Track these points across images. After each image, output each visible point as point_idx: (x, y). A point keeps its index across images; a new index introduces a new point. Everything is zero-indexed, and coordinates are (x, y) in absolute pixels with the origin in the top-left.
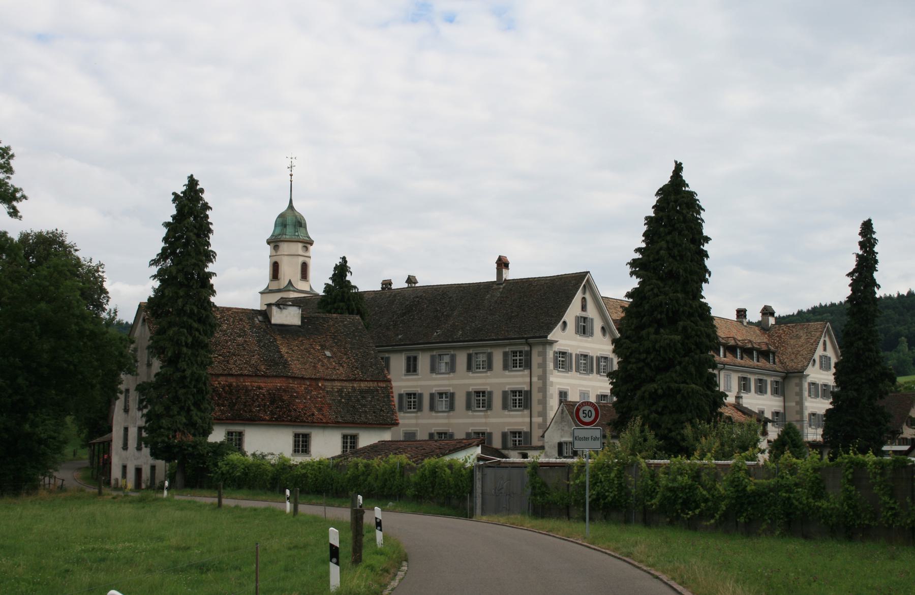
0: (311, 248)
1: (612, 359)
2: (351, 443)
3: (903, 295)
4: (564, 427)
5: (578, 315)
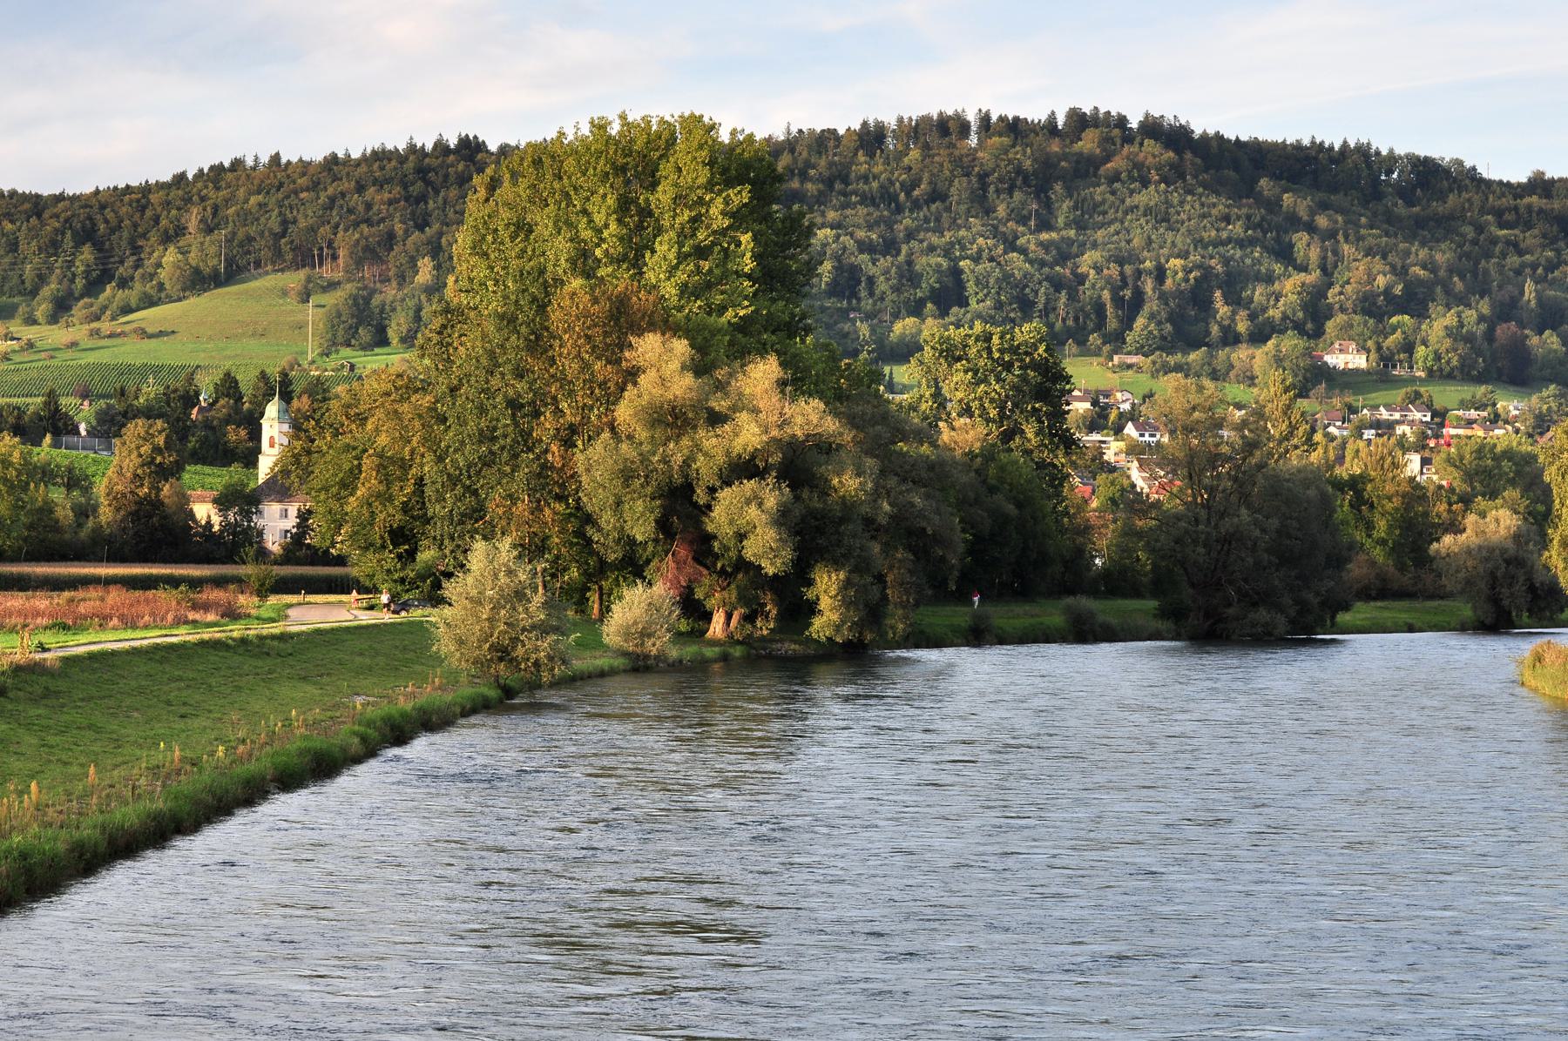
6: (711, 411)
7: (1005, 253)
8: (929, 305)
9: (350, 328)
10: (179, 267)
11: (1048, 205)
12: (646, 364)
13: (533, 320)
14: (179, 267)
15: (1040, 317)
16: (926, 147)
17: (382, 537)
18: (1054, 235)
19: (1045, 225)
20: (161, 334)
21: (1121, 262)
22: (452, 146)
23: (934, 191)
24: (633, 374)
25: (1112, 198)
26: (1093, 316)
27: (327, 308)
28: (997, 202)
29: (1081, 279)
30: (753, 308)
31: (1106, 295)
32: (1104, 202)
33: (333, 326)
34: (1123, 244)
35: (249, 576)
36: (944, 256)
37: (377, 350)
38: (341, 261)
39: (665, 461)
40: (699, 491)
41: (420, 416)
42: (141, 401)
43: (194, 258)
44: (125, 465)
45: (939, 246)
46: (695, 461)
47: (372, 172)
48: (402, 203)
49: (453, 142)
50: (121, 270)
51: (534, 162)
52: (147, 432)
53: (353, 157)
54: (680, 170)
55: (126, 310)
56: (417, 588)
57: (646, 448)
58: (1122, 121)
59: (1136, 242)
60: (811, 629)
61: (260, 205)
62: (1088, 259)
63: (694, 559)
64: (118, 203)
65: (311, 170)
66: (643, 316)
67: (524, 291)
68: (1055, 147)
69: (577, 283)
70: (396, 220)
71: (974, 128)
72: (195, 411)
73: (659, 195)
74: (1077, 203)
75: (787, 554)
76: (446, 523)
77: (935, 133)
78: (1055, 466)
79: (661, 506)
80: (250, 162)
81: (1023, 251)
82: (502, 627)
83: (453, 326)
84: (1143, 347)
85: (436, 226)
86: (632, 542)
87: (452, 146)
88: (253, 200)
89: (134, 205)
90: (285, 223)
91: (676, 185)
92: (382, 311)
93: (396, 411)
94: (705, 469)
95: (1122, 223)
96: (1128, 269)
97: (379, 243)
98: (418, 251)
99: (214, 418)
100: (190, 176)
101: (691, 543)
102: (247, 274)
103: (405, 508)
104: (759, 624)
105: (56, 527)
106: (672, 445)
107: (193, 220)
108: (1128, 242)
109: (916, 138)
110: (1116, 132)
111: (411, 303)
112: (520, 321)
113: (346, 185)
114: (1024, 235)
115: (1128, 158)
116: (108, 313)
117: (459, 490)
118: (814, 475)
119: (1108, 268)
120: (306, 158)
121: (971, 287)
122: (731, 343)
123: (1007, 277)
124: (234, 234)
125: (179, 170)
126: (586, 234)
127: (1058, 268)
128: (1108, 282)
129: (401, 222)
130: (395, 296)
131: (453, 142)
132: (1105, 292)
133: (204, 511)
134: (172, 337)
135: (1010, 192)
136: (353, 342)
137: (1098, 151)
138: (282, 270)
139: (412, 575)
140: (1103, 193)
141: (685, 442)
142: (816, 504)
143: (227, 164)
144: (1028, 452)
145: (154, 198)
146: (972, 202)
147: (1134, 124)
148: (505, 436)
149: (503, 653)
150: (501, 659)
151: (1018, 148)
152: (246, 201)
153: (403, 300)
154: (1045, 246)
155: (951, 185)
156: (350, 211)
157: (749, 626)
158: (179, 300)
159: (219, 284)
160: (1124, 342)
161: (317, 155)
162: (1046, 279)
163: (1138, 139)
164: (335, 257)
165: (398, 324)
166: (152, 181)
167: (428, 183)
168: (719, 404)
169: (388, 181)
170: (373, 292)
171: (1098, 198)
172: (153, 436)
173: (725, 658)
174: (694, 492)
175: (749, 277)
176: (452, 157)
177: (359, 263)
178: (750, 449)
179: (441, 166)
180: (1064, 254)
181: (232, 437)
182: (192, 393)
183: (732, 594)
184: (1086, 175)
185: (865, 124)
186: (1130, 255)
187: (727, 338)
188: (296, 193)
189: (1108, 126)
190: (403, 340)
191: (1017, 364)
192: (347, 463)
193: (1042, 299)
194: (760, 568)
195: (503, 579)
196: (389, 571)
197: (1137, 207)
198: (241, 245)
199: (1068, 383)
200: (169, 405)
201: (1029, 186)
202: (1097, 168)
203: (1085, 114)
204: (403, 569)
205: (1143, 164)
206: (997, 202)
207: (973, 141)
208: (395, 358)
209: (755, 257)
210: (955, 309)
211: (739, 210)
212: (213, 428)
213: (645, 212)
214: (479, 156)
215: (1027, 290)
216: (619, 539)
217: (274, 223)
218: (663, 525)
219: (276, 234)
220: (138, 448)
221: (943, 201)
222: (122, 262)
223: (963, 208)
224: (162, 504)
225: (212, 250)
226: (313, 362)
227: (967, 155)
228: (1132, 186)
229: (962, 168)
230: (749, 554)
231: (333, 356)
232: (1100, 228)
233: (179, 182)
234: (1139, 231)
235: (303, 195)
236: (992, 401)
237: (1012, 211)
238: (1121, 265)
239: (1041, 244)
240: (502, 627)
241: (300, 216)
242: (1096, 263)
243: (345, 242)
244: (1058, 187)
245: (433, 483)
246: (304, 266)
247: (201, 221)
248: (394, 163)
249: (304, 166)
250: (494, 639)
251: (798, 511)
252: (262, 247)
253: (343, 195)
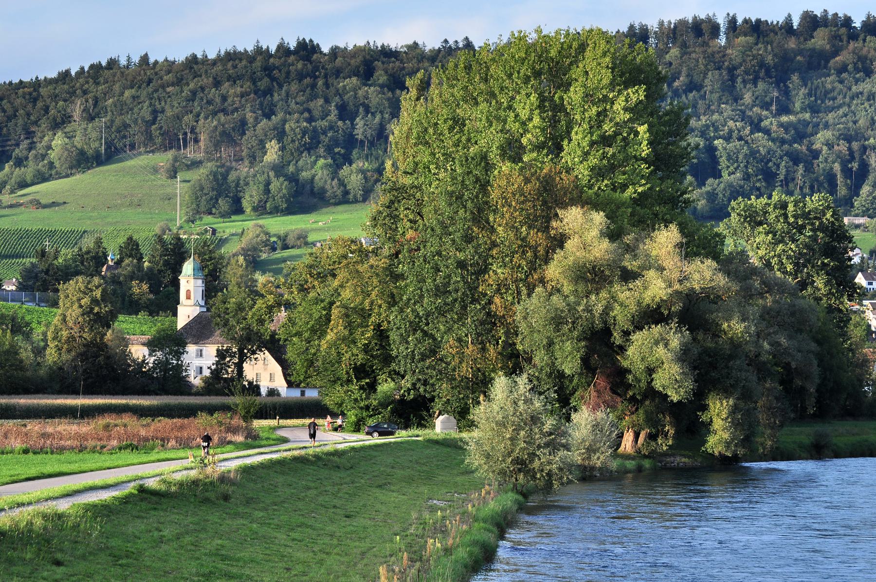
6: (624, 270)
7: (752, 133)
8: (689, 178)
9: (211, 199)
10: (67, 149)
11: (786, 93)
12: (571, 232)
13: (477, 197)
14: (67, 149)
15: (781, 186)
16: (684, 46)
17: (347, 373)
18: (792, 118)
19: (784, 109)
20: (54, 204)
21: (849, 139)
22: (292, 48)
23: (691, 82)
24: (560, 241)
25: (840, 86)
26: (826, 185)
27: (192, 183)
28: (744, 91)
29: (816, 154)
30: (649, 186)
31: (837, 167)
32: (833, 89)
33: (197, 198)
34: (850, 124)
35: (237, 405)
36: (701, 136)
37: (234, 218)
38: (202, 144)
39: (588, 310)
40: (615, 334)
41: (377, 275)
42: (60, 261)
43: (78, 141)
44: (68, 314)
45: (696, 128)
46: (612, 309)
47: (226, 70)
48: (252, 95)
49: (293, 45)
50: (17, 151)
51: (465, 68)
52: (86, 287)
53: (209, 57)
54: (587, 73)
55: (23, 185)
56: (379, 414)
57: (572, 299)
58: (847, 21)
59: (862, 122)
60: (707, 445)
61: (134, 97)
62: (822, 136)
63: (611, 389)
64: (13, 96)
65: (175, 68)
66: (565, 194)
67: (469, 173)
68: (792, 44)
69: (506, 167)
70: (248, 110)
71: (723, 29)
72: (104, 269)
73: (571, 94)
74: (811, 90)
75: (689, 384)
76: (408, 361)
77: (692, 35)
78: (840, 311)
79: (586, 346)
80: (123, 62)
81: (767, 132)
82: (523, 445)
83: (399, 202)
84: (868, 210)
85: (280, 115)
86: (561, 375)
87: (292, 48)
88: (128, 93)
89: (27, 97)
90: (155, 113)
91: (585, 86)
92: (237, 185)
93: (357, 271)
94: (620, 317)
95: (849, 106)
96: (855, 145)
97: (234, 129)
98: (266, 135)
99: (120, 274)
100: (73, 73)
101: (608, 376)
102: (124, 155)
103: (366, 349)
104: (660, 441)
105: (20, 366)
106: (593, 297)
107: (77, 110)
108: (855, 122)
109: (675, 38)
110: (843, 30)
111: (261, 178)
112: (466, 197)
113: (205, 80)
114: (767, 118)
115: (854, 52)
116: (8, 187)
117: (419, 334)
118: (706, 321)
119: (838, 145)
120: (171, 58)
121: (723, 162)
122: (632, 214)
123: (753, 153)
124: (112, 121)
125: (64, 69)
126: (515, 127)
127: (796, 145)
128: (838, 157)
129: (251, 111)
130: (248, 172)
131: (293, 45)
132: (836, 164)
133: (139, 352)
134: (62, 207)
135: (755, 82)
136: (214, 210)
137: (828, 47)
138: (153, 152)
139: (375, 403)
140: (832, 82)
141: (604, 294)
142: (710, 344)
143: (104, 64)
144: (818, 299)
145: (43, 91)
146: (723, 91)
147: (857, 24)
148: (457, 291)
149: (522, 465)
150: (520, 470)
151: (760, 45)
152: (122, 94)
153: (255, 176)
154: (786, 127)
155: (705, 78)
156: (209, 102)
157: (653, 443)
158: (67, 176)
159: (100, 163)
160: (852, 206)
161: (180, 56)
162: (785, 155)
163: (862, 36)
164: (196, 141)
165: (251, 196)
166: (41, 77)
167: (273, 79)
168: (630, 264)
169: (240, 77)
170: (230, 169)
171: (829, 86)
172: (91, 291)
173: (640, 469)
174: (612, 335)
175: (645, 160)
176: (292, 58)
177: (217, 145)
178: (657, 299)
179: (284, 64)
180: (801, 133)
181: (136, 290)
182: (101, 254)
183: (641, 415)
184: (818, 67)
185: (632, 27)
186: (857, 134)
187: (630, 210)
188: (163, 87)
189: (837, 25)
190: (255, 209)
191: (808, 227)
192: (317, 312)
193: (783, 171)
194: (666, 396)
195: (522, 406)
196: (356, 400)
197: (861, 93)
198: (118, 131)
199: (850, 242)
200: (82, 263)
201: (771, 77)
202: (827, 61)
203: (816, 16)
204: (368, 398)
205: (866, 58)
206: (744, 91)
207: (722, 40)
208: (250, 224)
209: (651, 143)
210: (710, 181)
211: (637, 105)
212: (120, 283)
213: (559, 108)
214: (315, 57)
215: (770, 164)
216: (551, 373)
217: (146, 113)
218: (585, 361)
219: (147, 122)
220: (79, 300)
221: (698, 91)
222: (18, 145)
223: (715, 96)
224: (106, 346)
225: (94, 135)
226: (181, 227)
227: (719, 52)
228: (858, 76)
229: (715, 63)
230: (658, 385)
231: (198, 222)
232: (830, 112)
233: (64, 78)
234: (864, 113)
235: (169, 89)
236: (789, 257)
237: (757, 98)
238: (849, 142)
239: (781, 125)
240: (523, 445)
241: (167, 107)
242: (828, 141)
243: (206, 128)
244: (795, 78)
245: (398, 328)
246: (171, 148)
247: (84, 110)
248: (244, 62)
249: (170, 65)
250: (515, 454)
251: (695, 351)
252: (136, 132)
253: (203, 89)
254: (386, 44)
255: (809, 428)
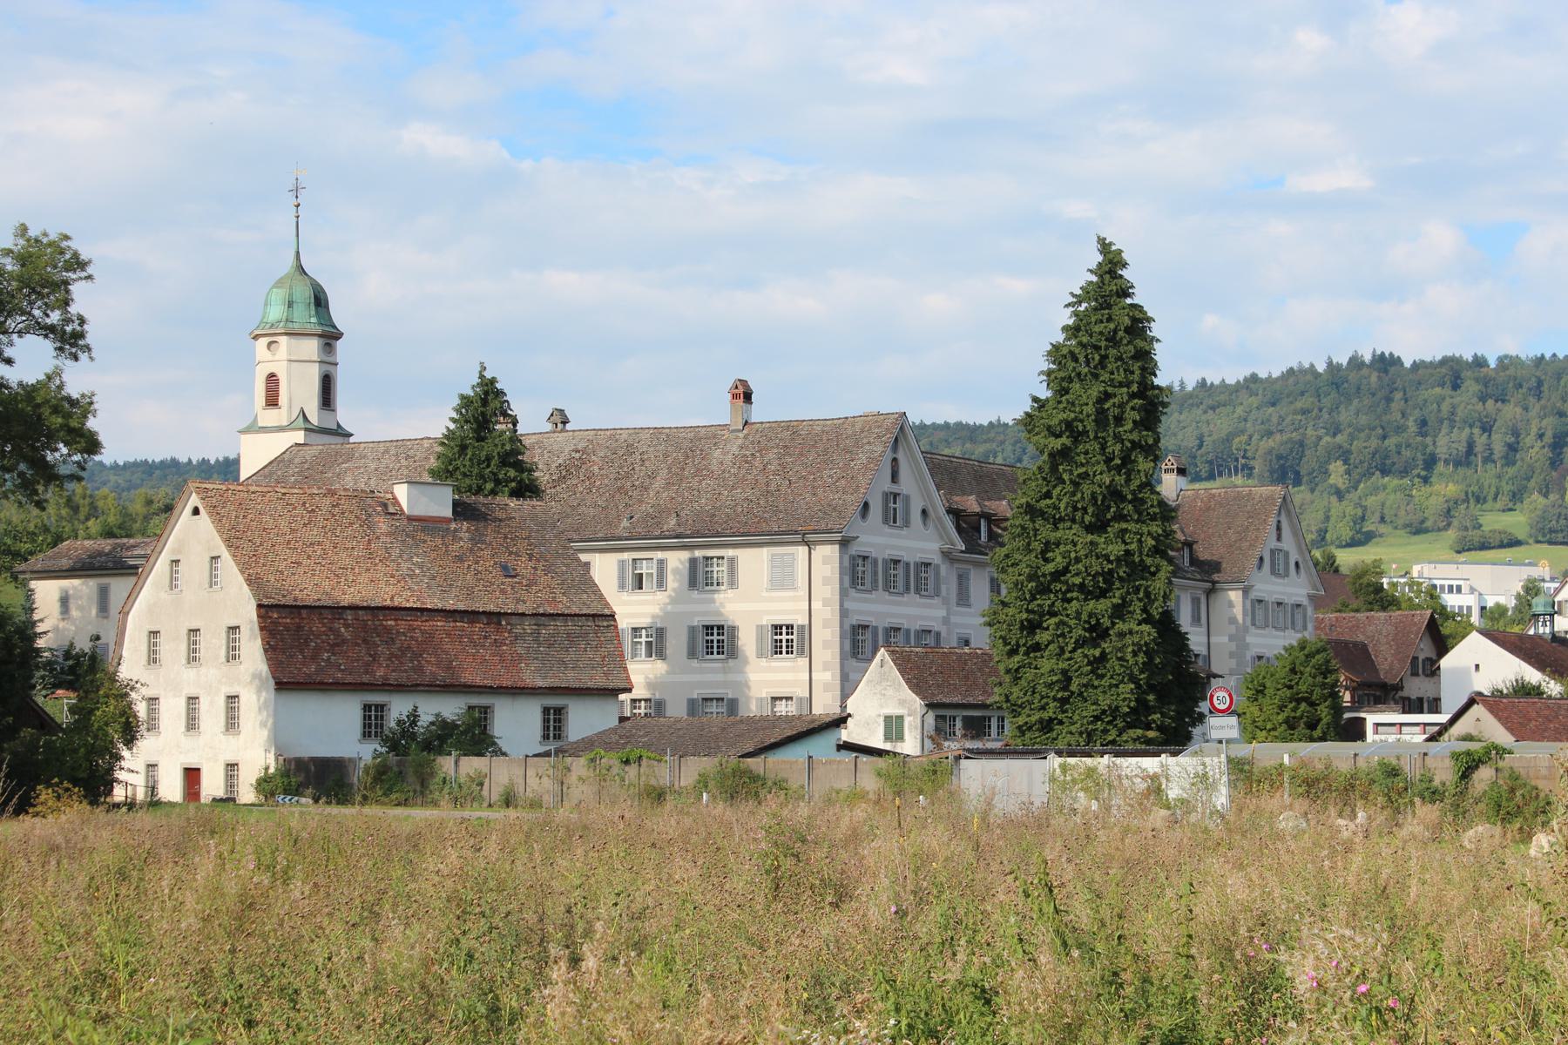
0: (339, 344)
1: (938, 566)
2: (555, 722)
3: (1339, 366)
4: (885, 689)
5: (886, 489)
49: (1368, 358)
53: (1274, 376)
131: (1368, 358)
161: (1438, 358)
254: (1479, 354)
255: (47, 709)
